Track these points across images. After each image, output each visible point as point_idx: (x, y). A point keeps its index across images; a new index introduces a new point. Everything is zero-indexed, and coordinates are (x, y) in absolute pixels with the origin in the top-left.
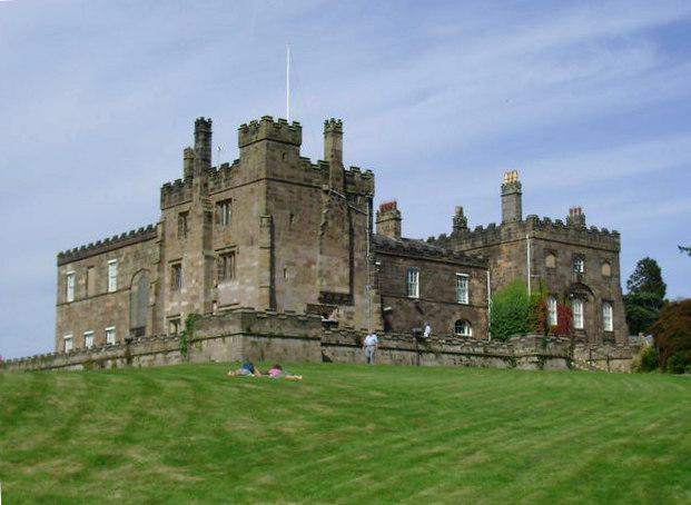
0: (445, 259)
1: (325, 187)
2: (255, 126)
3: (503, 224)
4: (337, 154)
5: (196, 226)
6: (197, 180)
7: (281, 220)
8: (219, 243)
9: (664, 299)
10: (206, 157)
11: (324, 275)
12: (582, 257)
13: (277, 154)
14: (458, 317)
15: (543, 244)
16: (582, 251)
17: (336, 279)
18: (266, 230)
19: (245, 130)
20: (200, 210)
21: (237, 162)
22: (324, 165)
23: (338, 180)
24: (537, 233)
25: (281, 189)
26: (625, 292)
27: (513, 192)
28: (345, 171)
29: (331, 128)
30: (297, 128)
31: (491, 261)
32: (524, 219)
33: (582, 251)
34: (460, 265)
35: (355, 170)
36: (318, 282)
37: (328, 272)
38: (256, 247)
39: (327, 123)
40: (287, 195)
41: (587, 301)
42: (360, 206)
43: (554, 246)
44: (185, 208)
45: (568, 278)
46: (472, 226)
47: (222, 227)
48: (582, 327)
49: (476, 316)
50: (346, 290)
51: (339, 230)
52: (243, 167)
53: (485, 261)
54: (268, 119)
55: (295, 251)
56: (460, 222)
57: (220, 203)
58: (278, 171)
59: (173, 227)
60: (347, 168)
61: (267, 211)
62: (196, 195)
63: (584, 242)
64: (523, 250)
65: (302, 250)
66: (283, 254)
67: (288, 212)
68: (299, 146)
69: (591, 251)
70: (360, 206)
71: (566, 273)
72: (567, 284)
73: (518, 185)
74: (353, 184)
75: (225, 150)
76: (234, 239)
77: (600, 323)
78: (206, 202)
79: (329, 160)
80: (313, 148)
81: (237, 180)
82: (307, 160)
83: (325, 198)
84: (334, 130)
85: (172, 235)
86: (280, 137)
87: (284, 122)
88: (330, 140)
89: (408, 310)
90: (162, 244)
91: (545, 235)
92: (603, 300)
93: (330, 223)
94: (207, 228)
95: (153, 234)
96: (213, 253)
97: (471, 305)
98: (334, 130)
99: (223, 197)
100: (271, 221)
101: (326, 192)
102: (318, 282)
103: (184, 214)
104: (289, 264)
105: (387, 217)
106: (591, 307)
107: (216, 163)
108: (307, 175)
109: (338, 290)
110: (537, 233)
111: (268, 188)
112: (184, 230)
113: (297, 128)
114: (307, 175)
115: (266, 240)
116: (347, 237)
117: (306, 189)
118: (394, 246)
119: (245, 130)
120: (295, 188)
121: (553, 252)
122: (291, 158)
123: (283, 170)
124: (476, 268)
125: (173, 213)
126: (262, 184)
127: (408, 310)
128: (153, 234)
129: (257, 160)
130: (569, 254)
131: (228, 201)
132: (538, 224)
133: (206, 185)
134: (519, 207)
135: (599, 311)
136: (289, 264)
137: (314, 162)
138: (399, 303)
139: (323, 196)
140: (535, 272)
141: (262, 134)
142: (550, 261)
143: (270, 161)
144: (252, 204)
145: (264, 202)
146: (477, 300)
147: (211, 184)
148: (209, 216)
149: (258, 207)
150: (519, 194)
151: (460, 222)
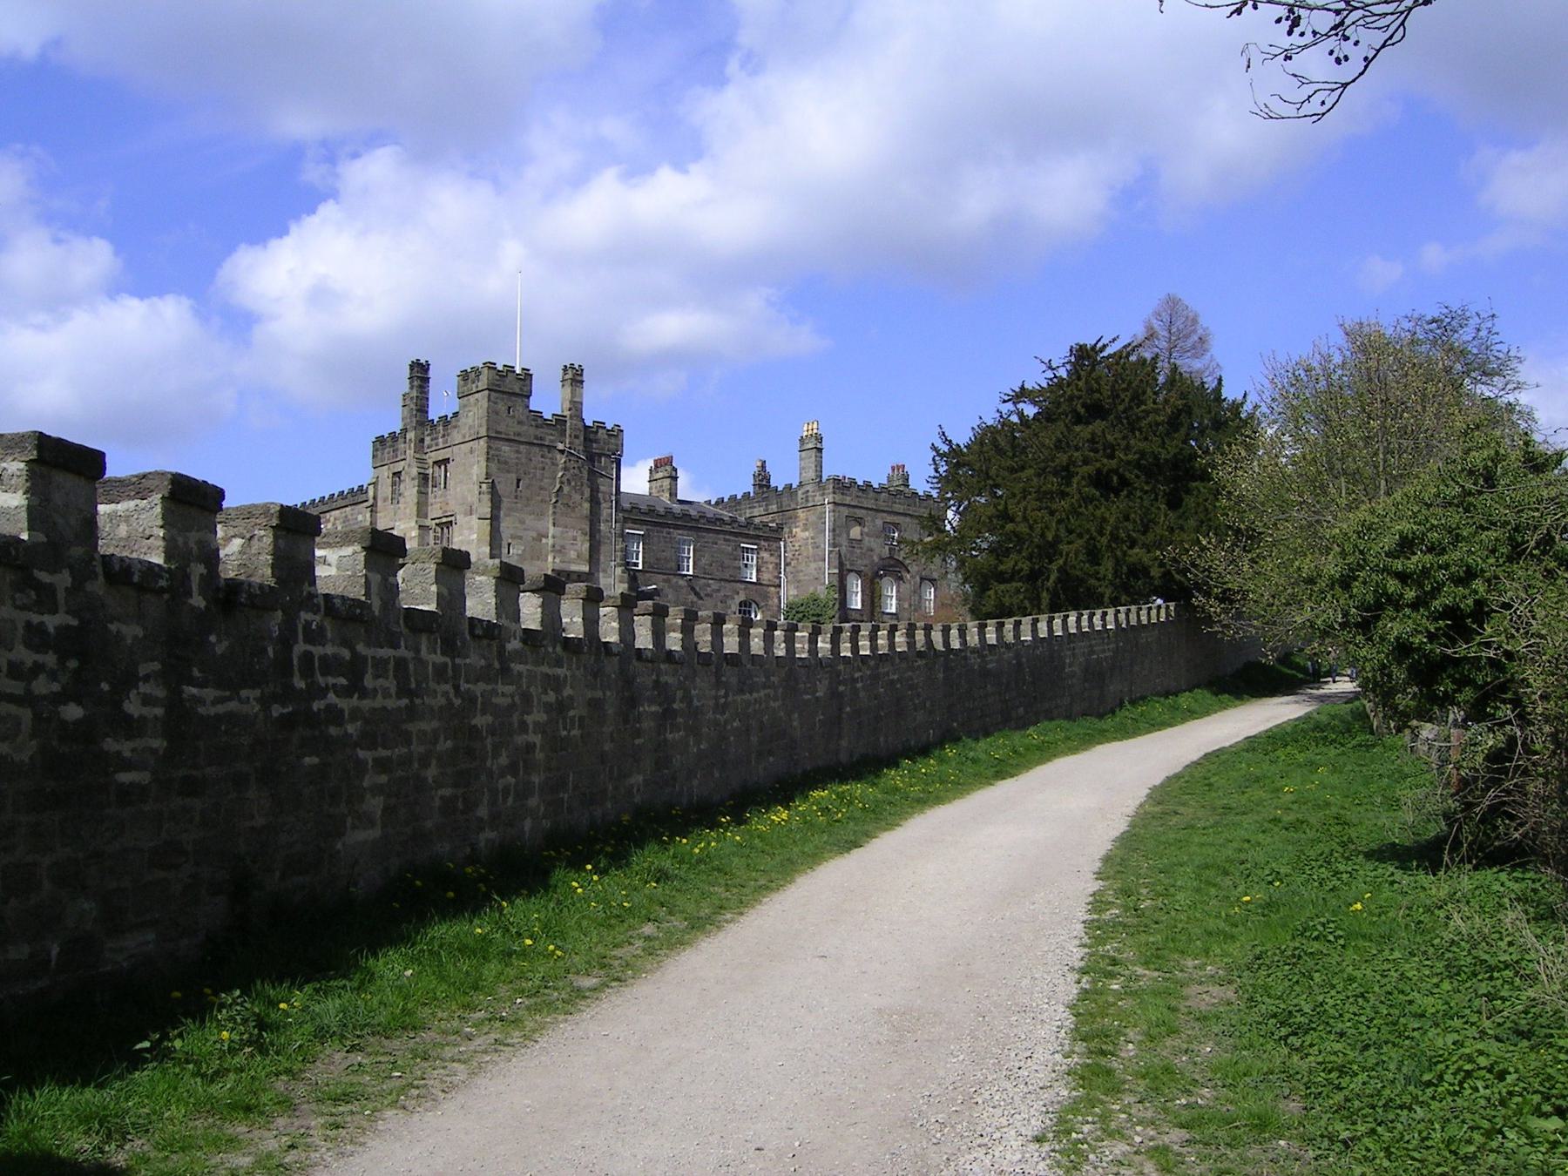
0: (727, 528)
1: (561, 446)
2: (477, 371)
3: (801, 485)
4: (576, 407)
5: (410, 490)
6: (411, 435)
7: (505, 486)
8: (434, 511)
9: (52, 630)
10: (422, 407)
11: (559, 550)
12: (897, 526)
13: (502, 407)
14: (742, 597)
15: (845, 511)
16: (896, 519)
17: (573, 554)
18: (486, 498)
19: (465, 376)
20: (415, 471)
21: (456, 414)
22: (560, 421)
23: (577, 437)
24: (838, 498)
25: (506, 448)
26: (113, 627)
27: (815, 446)
28: (586, 427)
29: (569, 376)
30: (527, 376)
31: (786, 530)
32: (824, 478)
33: (896, 519)
34: (747, 536)
35: (600, 425)
36: (550, 559)
37: (563, 547)
38: (474, 517)
39: (565, 369)
40: (514, 456)
41: (901, 578)
42: (605, 468)
43: (860, 513)
44: (399, 467)
45: (877, 551)
46: (778, 482)
47: (439, 492)
48: (893, 610)
49: (766, 597)
50: (585, 568)
51: (577, 497)
52: (463, 420)
53: (780, 528)
54: (491, 366)
55: (522, 522)
56: (762, 479)
57: (437, 463)
58: (502, 428)
59: (385, 490)
60: (589, 423)
61: (488, 475)
62: (410, 453)
63: (898, 508)
64: (822, 517)
65: (530, 520)
66: (506, 526)
67: (514, 476)
68: (528, 397)
69: (908, 519)
70: (605, 468)
71: (874, 545)
72: (876, 559)
73: (819, 439)
74: (596, 441)
75: (442, 401)
76: (453, 507)
77: (918, 606)
78: (421, 461)
79: (567, 413)
80: (548, 400)
81: (456, 437)
82: (538, 415)
83: (561, 459)
84: (574, 377)
85: (385, 500)
86: (508, 386)
87: (510, 369)
88: (568, 389)
89: (677, 588)
90: (373, 509)
91: (848, 500)
92: (922, 579)
93: (566, 489)
94: (422, 493)
95: (363, 497)
96: (428, 522)
97: (758, 583)
98: (574, 377)
99: (441, 455)
100: (493, 486)
101: (562, 452)
102: (550, 559)
103: (397, 474)
104: (513, 537)
105: (660, 475)
106: (905, 587)
107: (434, 414)
108: (539, 432)
109: (574, 568)
110: (838, 498)
111: (489, 447)
112: (396, 496)
113: (527, 376)
114: (539, 432)
115: (486, 510)
116: (587, 505)
117: (537, 449)
118: (662, 510)
119: (465, 376)
120: (522, 448)
121: (859, 521)
122: (519, 411)
123: (509, 427)
124: (767, 539)
125: (385, 473)
126: (482, 442)
127: (677, 588)
128: (363, 497)
129: (475, 416)
130: (879, 522)
131: (446, 461)
132: (841, 485)
133: (422, 441)
134: (819, 466)
135: (918, 591)
136: (513, 537)
137: (548, 416)
138: (667, 581)
139: (558, 456)
140: (834, 545)
141: (483, 383)
142: (855, 532)
143: (492, 414)
144: (471, 466)
145: (484, 464)
146: (766, 577)
147: (428, 440)
148: (424, 478)
149: (478, 469)
150: (820, 450)
151: (762, 479)
